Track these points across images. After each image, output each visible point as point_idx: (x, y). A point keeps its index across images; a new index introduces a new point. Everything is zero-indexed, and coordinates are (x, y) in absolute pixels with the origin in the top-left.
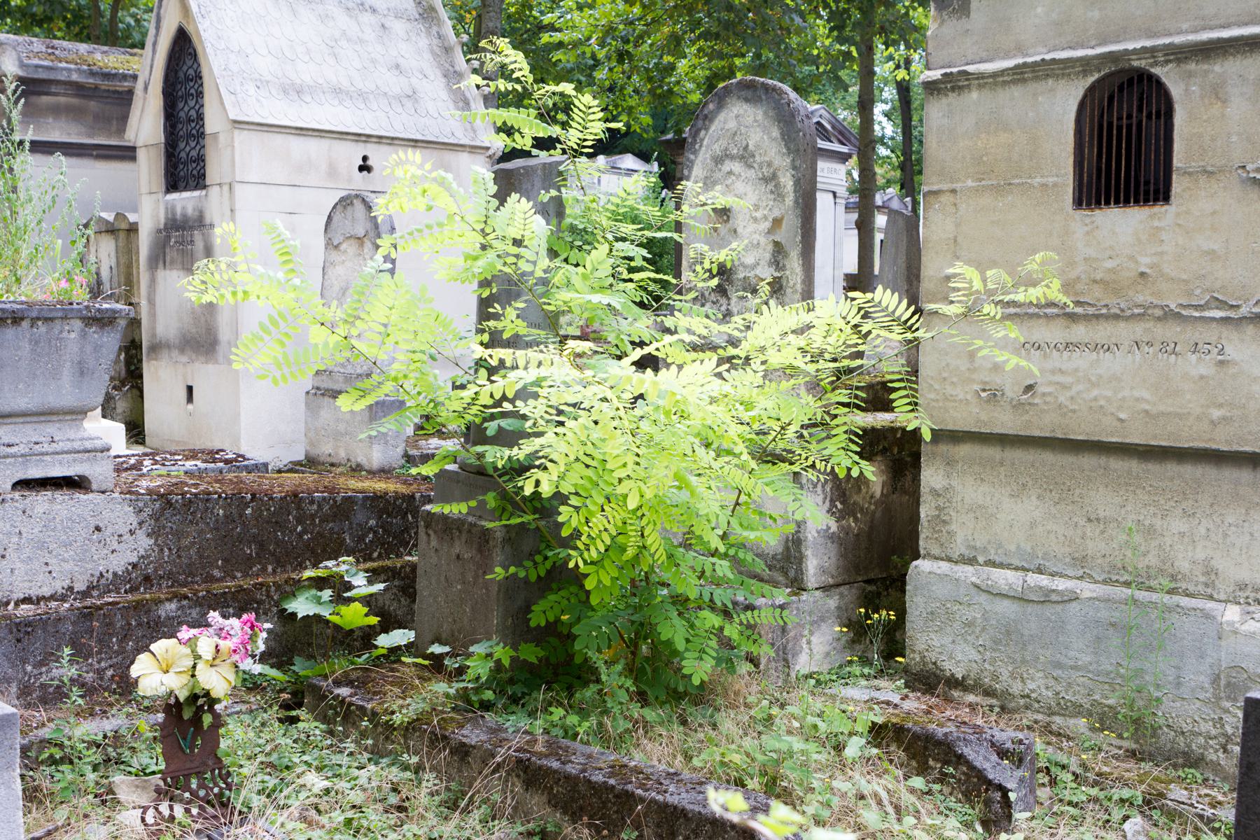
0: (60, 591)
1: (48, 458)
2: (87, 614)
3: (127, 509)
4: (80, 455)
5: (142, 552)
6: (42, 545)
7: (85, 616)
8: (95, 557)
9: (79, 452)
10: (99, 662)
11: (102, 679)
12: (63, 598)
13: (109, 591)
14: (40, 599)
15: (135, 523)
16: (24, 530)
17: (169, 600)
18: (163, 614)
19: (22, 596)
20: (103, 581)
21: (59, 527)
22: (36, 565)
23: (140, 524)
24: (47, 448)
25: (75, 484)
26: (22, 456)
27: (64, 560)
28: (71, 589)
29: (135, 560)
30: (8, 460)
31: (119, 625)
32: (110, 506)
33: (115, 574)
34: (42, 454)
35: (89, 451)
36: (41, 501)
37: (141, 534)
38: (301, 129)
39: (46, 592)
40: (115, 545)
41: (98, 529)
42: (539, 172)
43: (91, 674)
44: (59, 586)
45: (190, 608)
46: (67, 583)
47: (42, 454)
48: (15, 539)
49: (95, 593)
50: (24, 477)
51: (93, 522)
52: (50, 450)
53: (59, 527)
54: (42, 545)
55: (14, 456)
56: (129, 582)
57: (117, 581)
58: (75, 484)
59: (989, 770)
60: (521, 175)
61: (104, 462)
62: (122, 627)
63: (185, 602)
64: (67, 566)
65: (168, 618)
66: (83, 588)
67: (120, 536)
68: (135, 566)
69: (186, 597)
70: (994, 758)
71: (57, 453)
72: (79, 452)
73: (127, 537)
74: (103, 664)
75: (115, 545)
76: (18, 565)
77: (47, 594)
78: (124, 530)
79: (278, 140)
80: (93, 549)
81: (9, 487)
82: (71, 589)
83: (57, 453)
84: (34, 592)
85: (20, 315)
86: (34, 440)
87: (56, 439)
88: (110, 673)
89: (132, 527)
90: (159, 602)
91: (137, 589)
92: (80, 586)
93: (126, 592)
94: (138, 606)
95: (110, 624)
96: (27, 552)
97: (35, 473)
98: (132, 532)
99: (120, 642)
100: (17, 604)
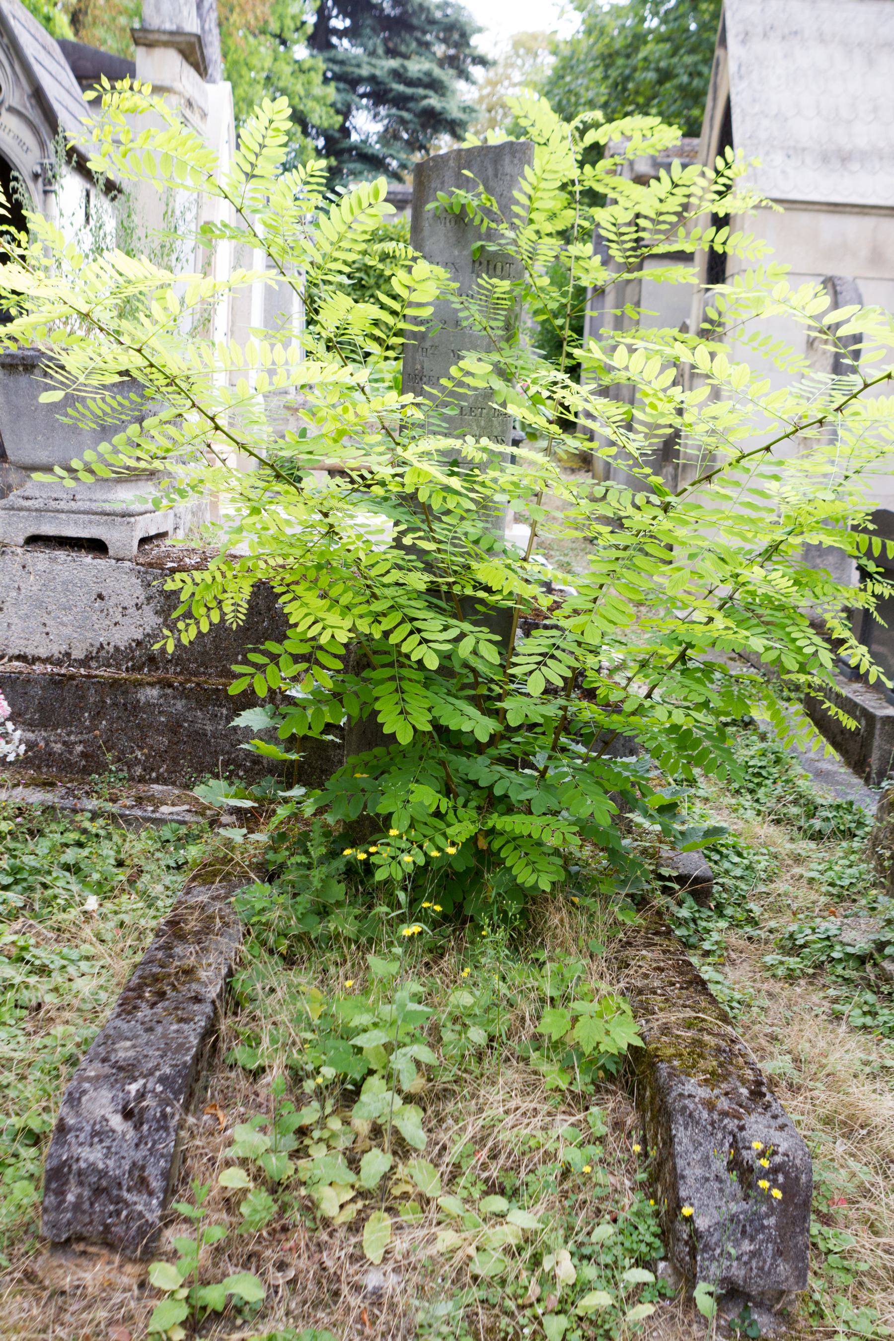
0: (57, 655)
1: (63, 516)
2: (57, 682)
3: (134, 580)
4: (97, 517)
5: (148, 630)
6: (40, 604)
7: (55, 683)
8: (96, 627)
9: (96, 513)
10: (69, 735)
11: (71, 753)
12: (59, 663)
13: (109, 666)
14: (36, 659)
15: (142, 597)
16: (23, 586)
17: (152, 685)
18: (143, 699)
19: (17, 652)
20: (103, 653)
21: (59, 588)
22: (33, 623)
23: (149, 599)
24: (62, 505)
25: (97, 547)
26: (36, 510)
27: (63, 624)
28: (68, 654)
29: (140, 637)
30: (22, 513)
31: (92, 700)
32: (115, 574)
33: (117, 648)
34: (58, 511)
35: (108, 515)
36: (41, 558)
37: (148, 610)
38: (836, 205)
39: (43, 653)
40: (119, 618)
41: (100, 597)
42: (452, 163)
43: (59, 745)
44: (56, 649)
45: (174, 698)
46: (64, 648)
47: (58, 511)
48: (14, 594)
49: (94, 664)
50: (37, 532)
51: (96, 589)
52: (66, 508)
53: (59, 588)
54: (40, 604)
55: (28, 510)
56: (132, 659)
57: (117, 657)
58: (97, 547)
59: (690, 1181)
60: (431, 169)
61: (123, 528)
62: (95, 703)
63: (169, 691)
64: (67, 631)
65: (148, 704)
66: (82, 657)
67: (125, 608)
68: (139, 643)
69: (170, 686)
70: (719, 1165)
71: (73, 512)
72: (96, 513)
73: (132, 611)
74: (72, 738)
75: (119, 618)
76: (15, 620)
77: (44, 656)
78: (130, 603)
79: (805, 219)
80: (95, 618)
81: (21, 541)
82: (68, 654)
83: (73, 512)
84: (30, 651)
85: (29, 362)
86: (55, 495)
87: (78, 497)
88: (79, 748)
89: (139, 601)
90: (139, 684)
91: (140, 669)
92: (78, 654)
93: (127, 670)
94: (115, 684)
95: (83, 698)
96: (25, 609)
97: (49, 529)
98: (138, 607)
99: (92, 719)
100: (10, 660)
